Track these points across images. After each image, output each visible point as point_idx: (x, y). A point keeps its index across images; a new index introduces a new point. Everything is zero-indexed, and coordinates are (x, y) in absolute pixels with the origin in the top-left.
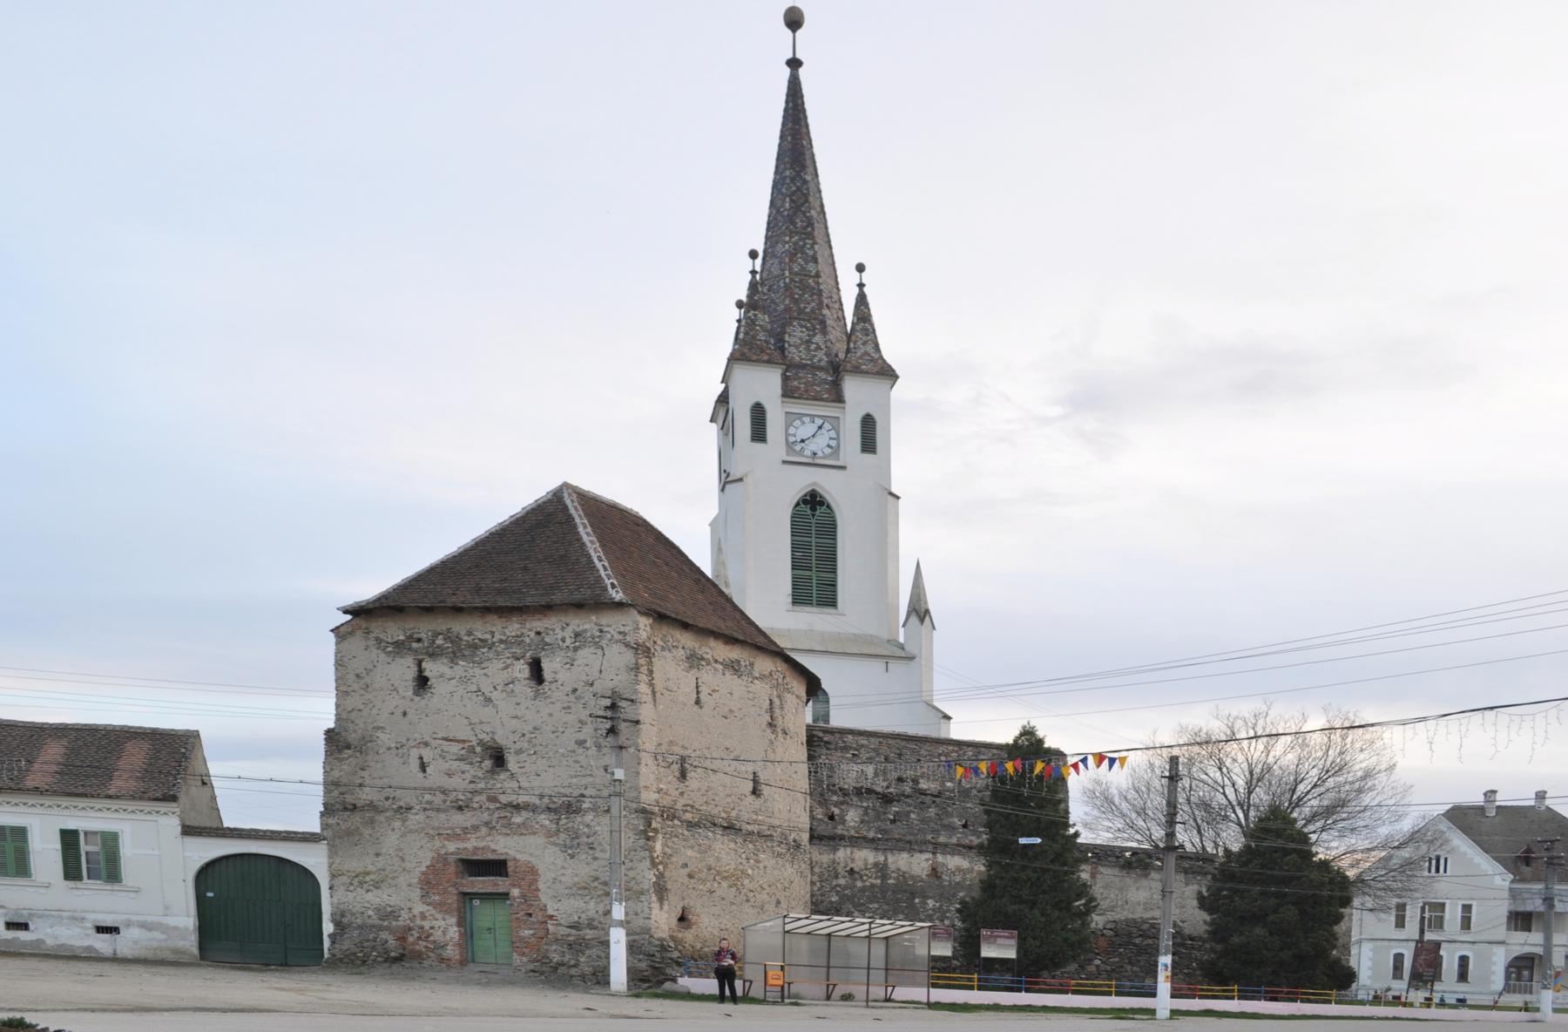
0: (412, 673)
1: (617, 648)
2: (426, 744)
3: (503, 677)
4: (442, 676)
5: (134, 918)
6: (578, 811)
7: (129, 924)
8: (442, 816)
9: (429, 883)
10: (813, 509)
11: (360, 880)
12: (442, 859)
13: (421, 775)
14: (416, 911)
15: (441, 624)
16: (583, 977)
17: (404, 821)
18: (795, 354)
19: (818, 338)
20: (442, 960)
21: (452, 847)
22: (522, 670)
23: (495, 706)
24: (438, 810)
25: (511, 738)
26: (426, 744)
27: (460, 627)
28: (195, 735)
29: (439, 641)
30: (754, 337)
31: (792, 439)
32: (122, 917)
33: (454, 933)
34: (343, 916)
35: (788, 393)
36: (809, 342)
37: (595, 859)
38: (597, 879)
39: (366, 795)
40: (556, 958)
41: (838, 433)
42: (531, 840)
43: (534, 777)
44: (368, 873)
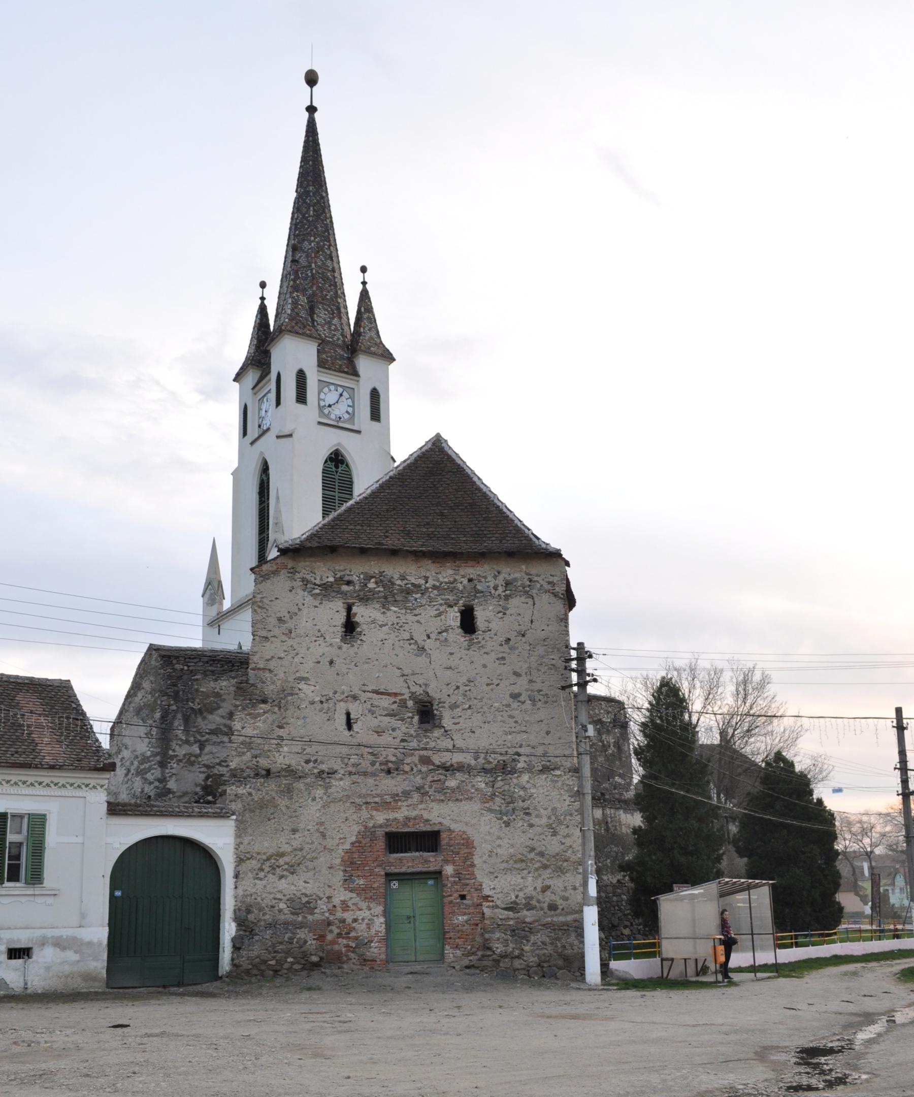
0: (341, 618)
1: (546, 598)
2: (355, 698)
3: (434, 625)
4: (373, 622)
5: (49, 933)
6: (513, 771)
7: (43, 942)
8: (371, 781)
9: (352, 864)
10: (337, 467)
11: (273, 864)
12: (368, 833)
13: (347, 733)
14: (336, 901)
15: (373, 566)
16: (528, 971)
17: (327, 787)
18: (324, 332)
19: (335, 321)
20: (364, 961)
21: (380, 817)
22: (453, 617)
23: (429, 656)
24: (365, 774)
25: (445, 691)
26: (355, 698)
27: (394, 570)
28: (69, 681)
29: (372, 585)
30: (298, 314)
31: (322, 404)
32: (38, 933)
33: (379, 924)
34: (249, 911)
35: (322, 364)
36: (330, 323)
37: (531, 826)
38: (532, 849)
39: (285, 757)
40: (499, 948)
41: (353, 402)
42: (466, 806)
43: (471, 733)
44: (282, 855)
